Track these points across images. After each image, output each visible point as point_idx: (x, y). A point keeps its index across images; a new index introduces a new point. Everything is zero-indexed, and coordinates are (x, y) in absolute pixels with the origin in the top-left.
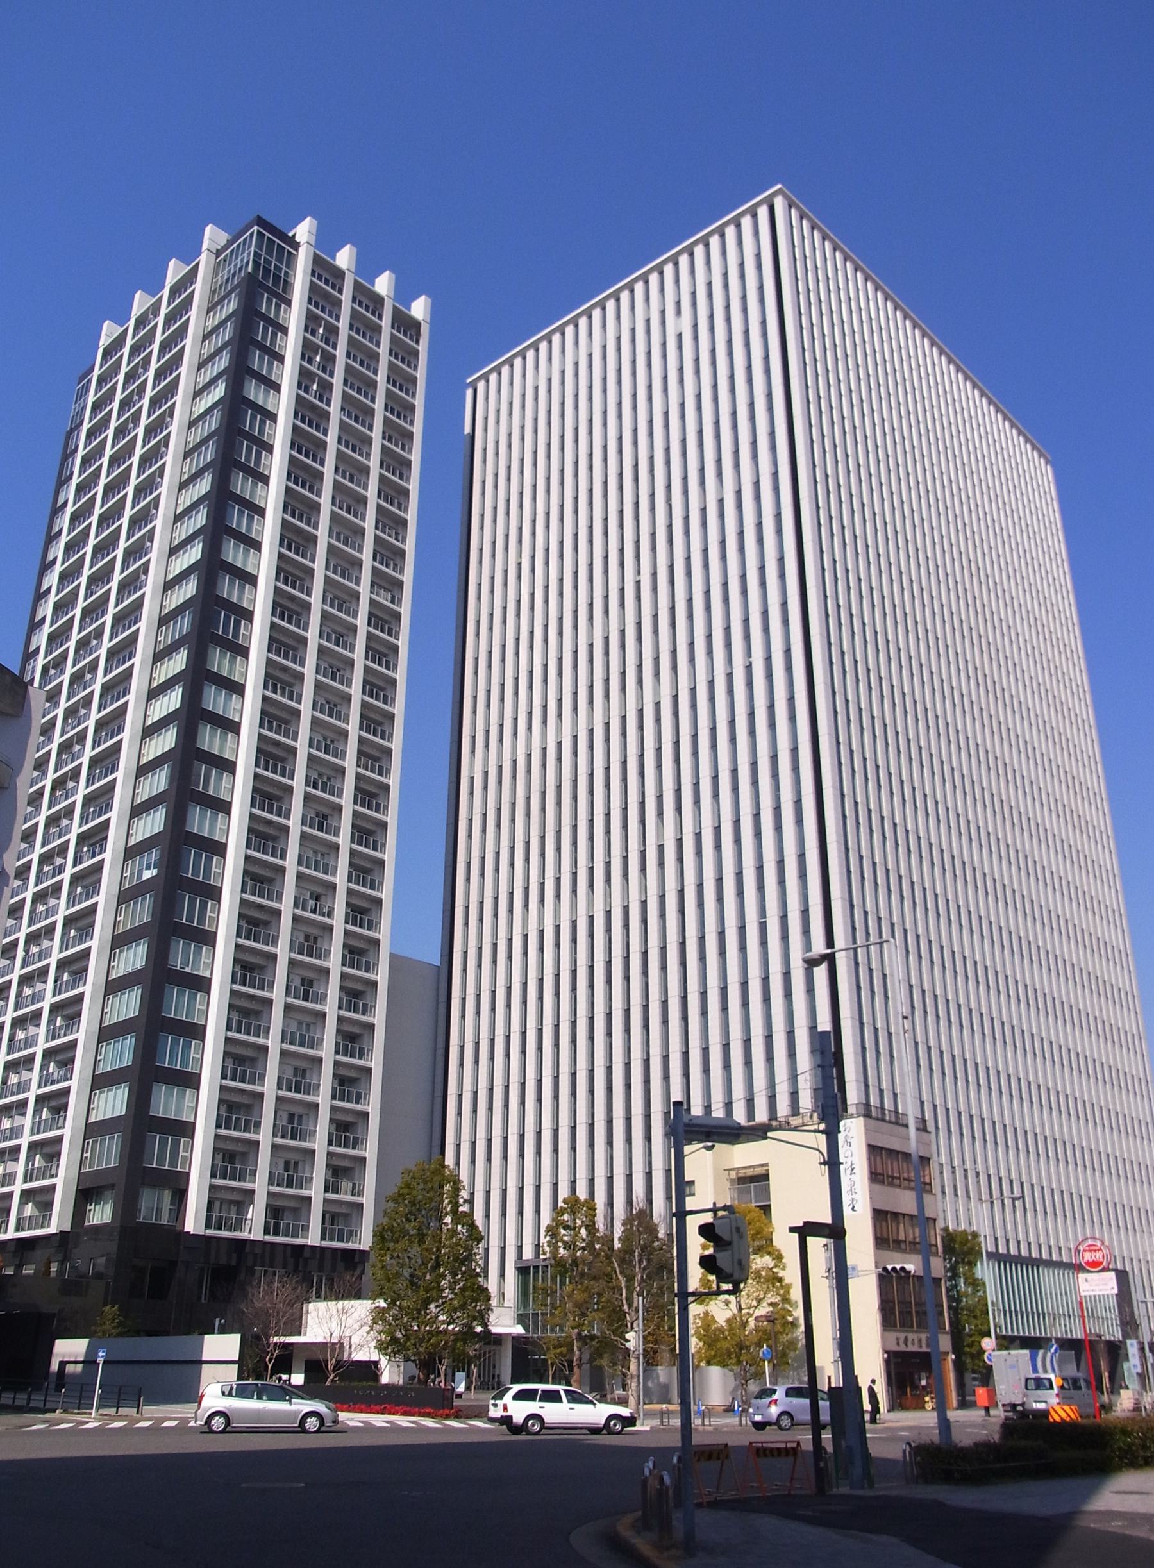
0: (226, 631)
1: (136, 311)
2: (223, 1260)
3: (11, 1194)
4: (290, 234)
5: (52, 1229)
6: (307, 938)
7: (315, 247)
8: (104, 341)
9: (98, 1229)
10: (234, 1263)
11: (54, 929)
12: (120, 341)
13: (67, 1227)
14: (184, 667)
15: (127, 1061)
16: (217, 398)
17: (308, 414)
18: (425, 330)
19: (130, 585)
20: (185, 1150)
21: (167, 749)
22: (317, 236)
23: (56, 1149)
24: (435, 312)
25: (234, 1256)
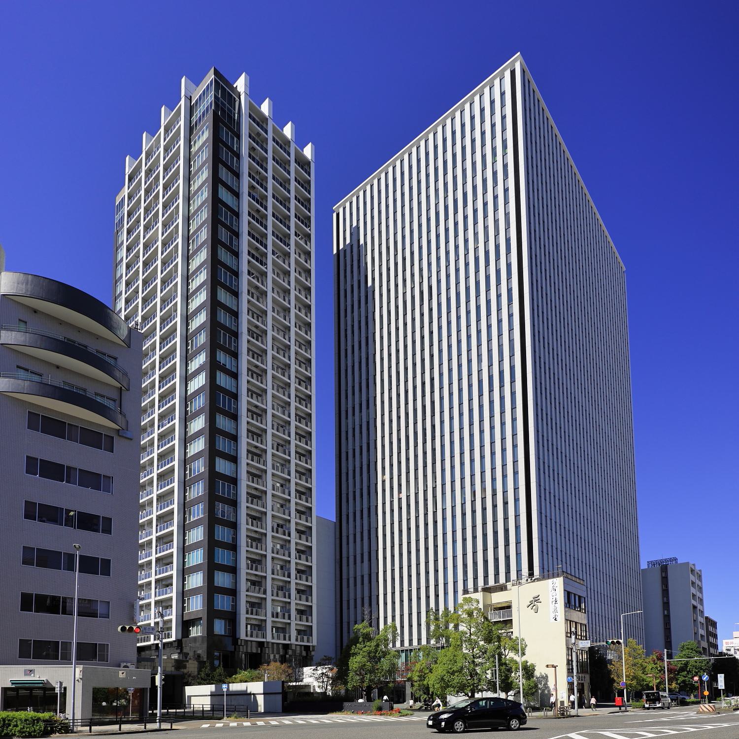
0: (224, 405)
1: (145, 148)
2: (254, 651)
3: (151, 561)
4: (235, 86)
5: (173, 638)
6: (278, 525)
7: (250, 96)
8: (128, 171)
9: (195, 638)
10: (259, 652)
11: (152, 522)
12: (137, 170)
13: (180, 637)
14: (204, 383)
15: (201, 538)
16: (202, 281)
17: (253, 290)
18: (313, 165)
19: (166, 338)
20: (235, 342)
21: (201, 385)
22: (250, 88)
23: (170, 539)
24: (316, 152)
25: (259, 649)
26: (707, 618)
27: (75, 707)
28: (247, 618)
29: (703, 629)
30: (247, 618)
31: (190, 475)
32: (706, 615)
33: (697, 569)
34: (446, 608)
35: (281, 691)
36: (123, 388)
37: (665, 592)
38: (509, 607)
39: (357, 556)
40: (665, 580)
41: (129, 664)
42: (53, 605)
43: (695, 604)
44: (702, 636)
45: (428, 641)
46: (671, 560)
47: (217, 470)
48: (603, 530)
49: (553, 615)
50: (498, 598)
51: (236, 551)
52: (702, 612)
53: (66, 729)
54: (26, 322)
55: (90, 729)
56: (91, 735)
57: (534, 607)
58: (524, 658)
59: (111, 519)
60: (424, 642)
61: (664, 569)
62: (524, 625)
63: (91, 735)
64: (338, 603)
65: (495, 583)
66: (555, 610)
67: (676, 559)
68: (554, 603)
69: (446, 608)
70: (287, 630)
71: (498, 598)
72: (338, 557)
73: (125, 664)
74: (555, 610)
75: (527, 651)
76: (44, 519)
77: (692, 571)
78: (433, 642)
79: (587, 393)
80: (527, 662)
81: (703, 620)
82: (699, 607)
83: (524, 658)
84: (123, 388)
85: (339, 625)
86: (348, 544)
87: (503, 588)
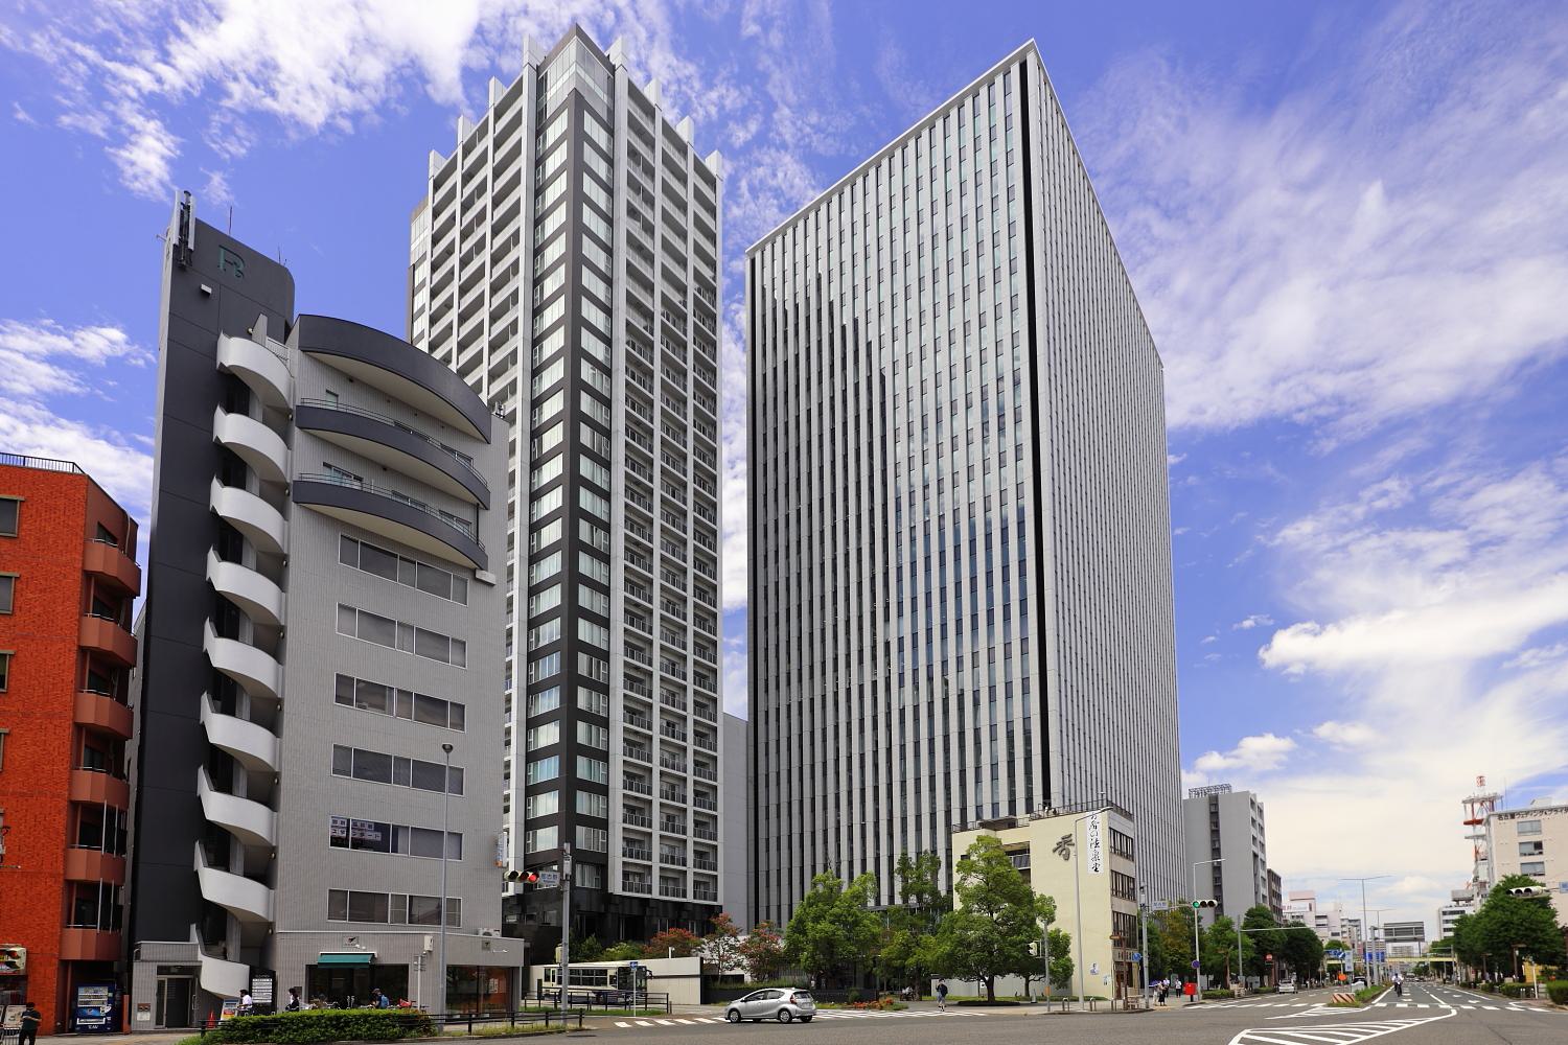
6: (668, 724)
8: (434, 172)
14: (560, 504)
26: (1270, 872)
27: (426, 993)
28: (624, 863)
29: (1265, 887)
30: (624, 863)
31: (537, 644)
32: (1268, 867)
33: (1259, 800)
34: (904, 854)
35: (699, 973)
36: (481, 505)
37: (1215, 832)
38: (1519, 833)
39: (781, 772)
40: (1214, 815)
41: (491, 931)
42: (384, 838)
43: (1256, 851)
44: (1264, 897)
45: (905, 900)
46: (1222, 787)
47: (581, 637)
48: (1098, 744)
49: (1092, 864)
50: (1008, 837)
51: (607, 761)
52: (1264, 863)
53: (417, 1024)
54: (337, 396)
55: (547, 1023)
56: (470, 1039)
57: (1064, 853)
58: (1051, 927)
59: (464, 706)
60: (898, 900)
61: (1214, 802)
62: (1046, 878)
63: (470, 1039)
64: (752, 843)
65: (993, 817)
66: (1096, 857)
67: (1228, 787)
68: (1093, 846)
69: (904, 854)
70: (681, 880)
71: (1008, 837)
72: (752, 774)
73: (485, 930)
74: (1096, 857)
75: (1058, 914)
76: (364, 704)
77: (1253, 803)
78: (913, 899)
79: (1070, 543)
80: (1059, 931)
81: (1265, 876)
82: (1260, 855)
83: (1051, 927)
84: (481, 505)
85: (752, 875)
86: (767, 754)
87: (1011, 824)
